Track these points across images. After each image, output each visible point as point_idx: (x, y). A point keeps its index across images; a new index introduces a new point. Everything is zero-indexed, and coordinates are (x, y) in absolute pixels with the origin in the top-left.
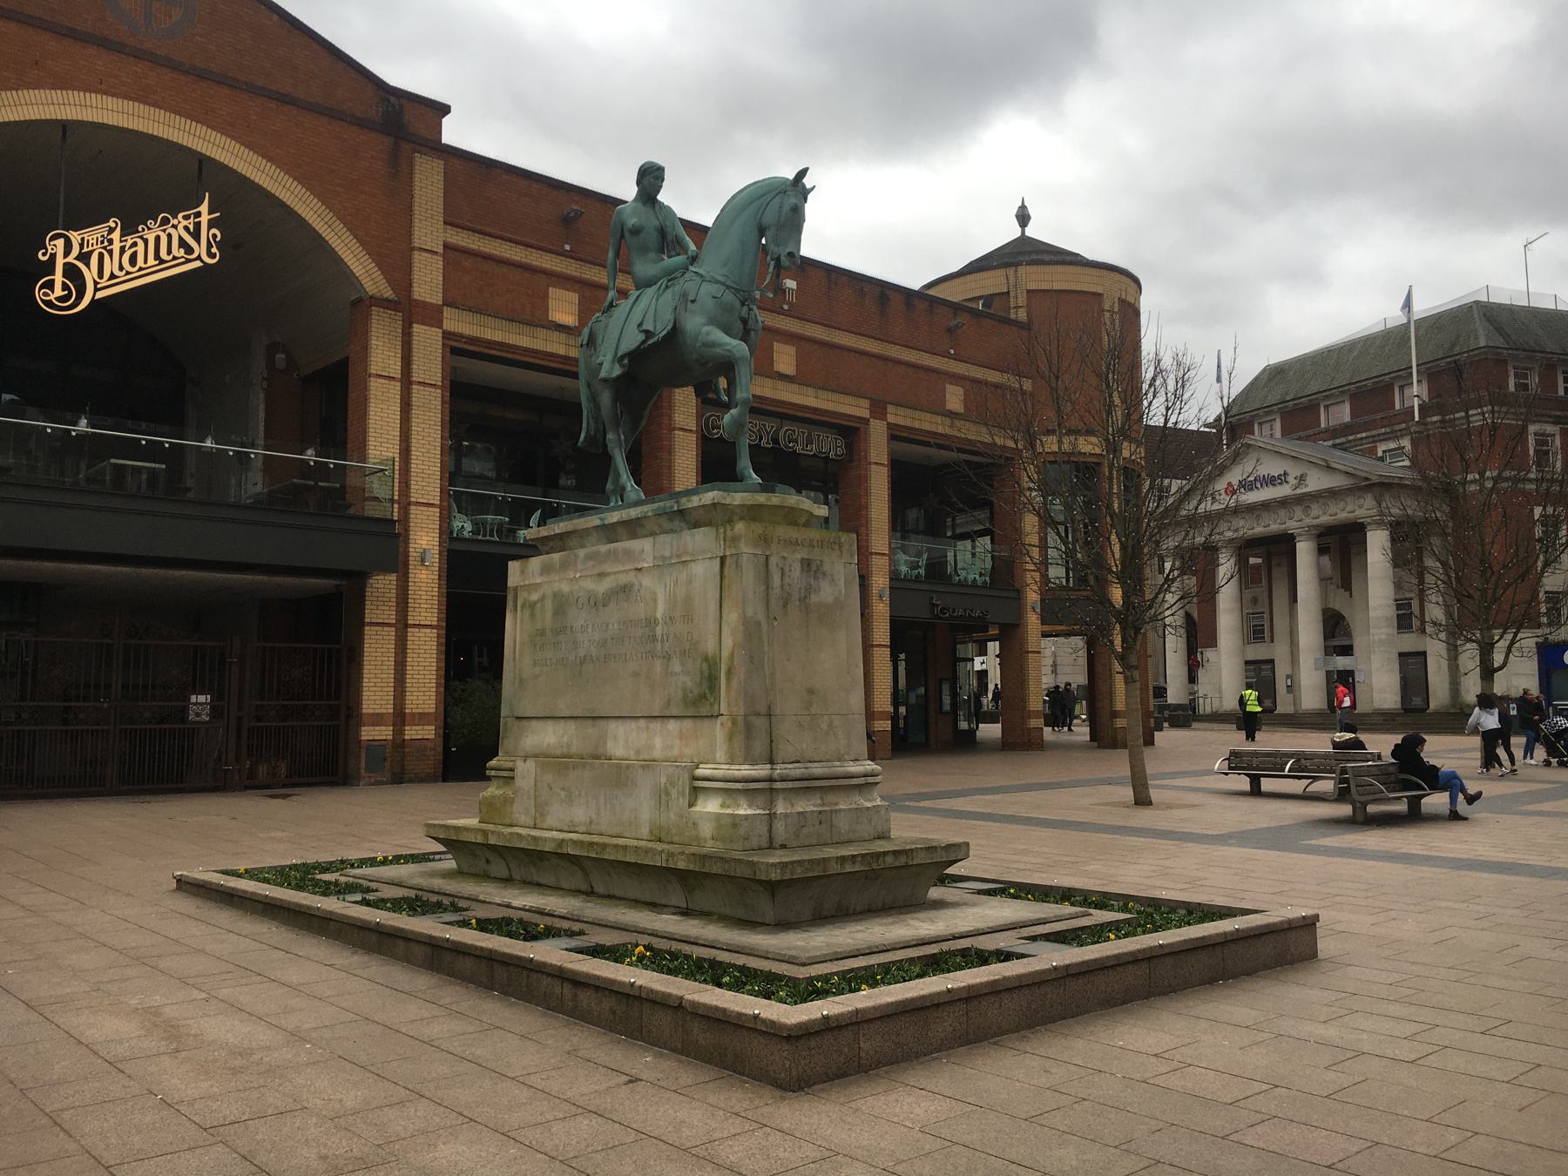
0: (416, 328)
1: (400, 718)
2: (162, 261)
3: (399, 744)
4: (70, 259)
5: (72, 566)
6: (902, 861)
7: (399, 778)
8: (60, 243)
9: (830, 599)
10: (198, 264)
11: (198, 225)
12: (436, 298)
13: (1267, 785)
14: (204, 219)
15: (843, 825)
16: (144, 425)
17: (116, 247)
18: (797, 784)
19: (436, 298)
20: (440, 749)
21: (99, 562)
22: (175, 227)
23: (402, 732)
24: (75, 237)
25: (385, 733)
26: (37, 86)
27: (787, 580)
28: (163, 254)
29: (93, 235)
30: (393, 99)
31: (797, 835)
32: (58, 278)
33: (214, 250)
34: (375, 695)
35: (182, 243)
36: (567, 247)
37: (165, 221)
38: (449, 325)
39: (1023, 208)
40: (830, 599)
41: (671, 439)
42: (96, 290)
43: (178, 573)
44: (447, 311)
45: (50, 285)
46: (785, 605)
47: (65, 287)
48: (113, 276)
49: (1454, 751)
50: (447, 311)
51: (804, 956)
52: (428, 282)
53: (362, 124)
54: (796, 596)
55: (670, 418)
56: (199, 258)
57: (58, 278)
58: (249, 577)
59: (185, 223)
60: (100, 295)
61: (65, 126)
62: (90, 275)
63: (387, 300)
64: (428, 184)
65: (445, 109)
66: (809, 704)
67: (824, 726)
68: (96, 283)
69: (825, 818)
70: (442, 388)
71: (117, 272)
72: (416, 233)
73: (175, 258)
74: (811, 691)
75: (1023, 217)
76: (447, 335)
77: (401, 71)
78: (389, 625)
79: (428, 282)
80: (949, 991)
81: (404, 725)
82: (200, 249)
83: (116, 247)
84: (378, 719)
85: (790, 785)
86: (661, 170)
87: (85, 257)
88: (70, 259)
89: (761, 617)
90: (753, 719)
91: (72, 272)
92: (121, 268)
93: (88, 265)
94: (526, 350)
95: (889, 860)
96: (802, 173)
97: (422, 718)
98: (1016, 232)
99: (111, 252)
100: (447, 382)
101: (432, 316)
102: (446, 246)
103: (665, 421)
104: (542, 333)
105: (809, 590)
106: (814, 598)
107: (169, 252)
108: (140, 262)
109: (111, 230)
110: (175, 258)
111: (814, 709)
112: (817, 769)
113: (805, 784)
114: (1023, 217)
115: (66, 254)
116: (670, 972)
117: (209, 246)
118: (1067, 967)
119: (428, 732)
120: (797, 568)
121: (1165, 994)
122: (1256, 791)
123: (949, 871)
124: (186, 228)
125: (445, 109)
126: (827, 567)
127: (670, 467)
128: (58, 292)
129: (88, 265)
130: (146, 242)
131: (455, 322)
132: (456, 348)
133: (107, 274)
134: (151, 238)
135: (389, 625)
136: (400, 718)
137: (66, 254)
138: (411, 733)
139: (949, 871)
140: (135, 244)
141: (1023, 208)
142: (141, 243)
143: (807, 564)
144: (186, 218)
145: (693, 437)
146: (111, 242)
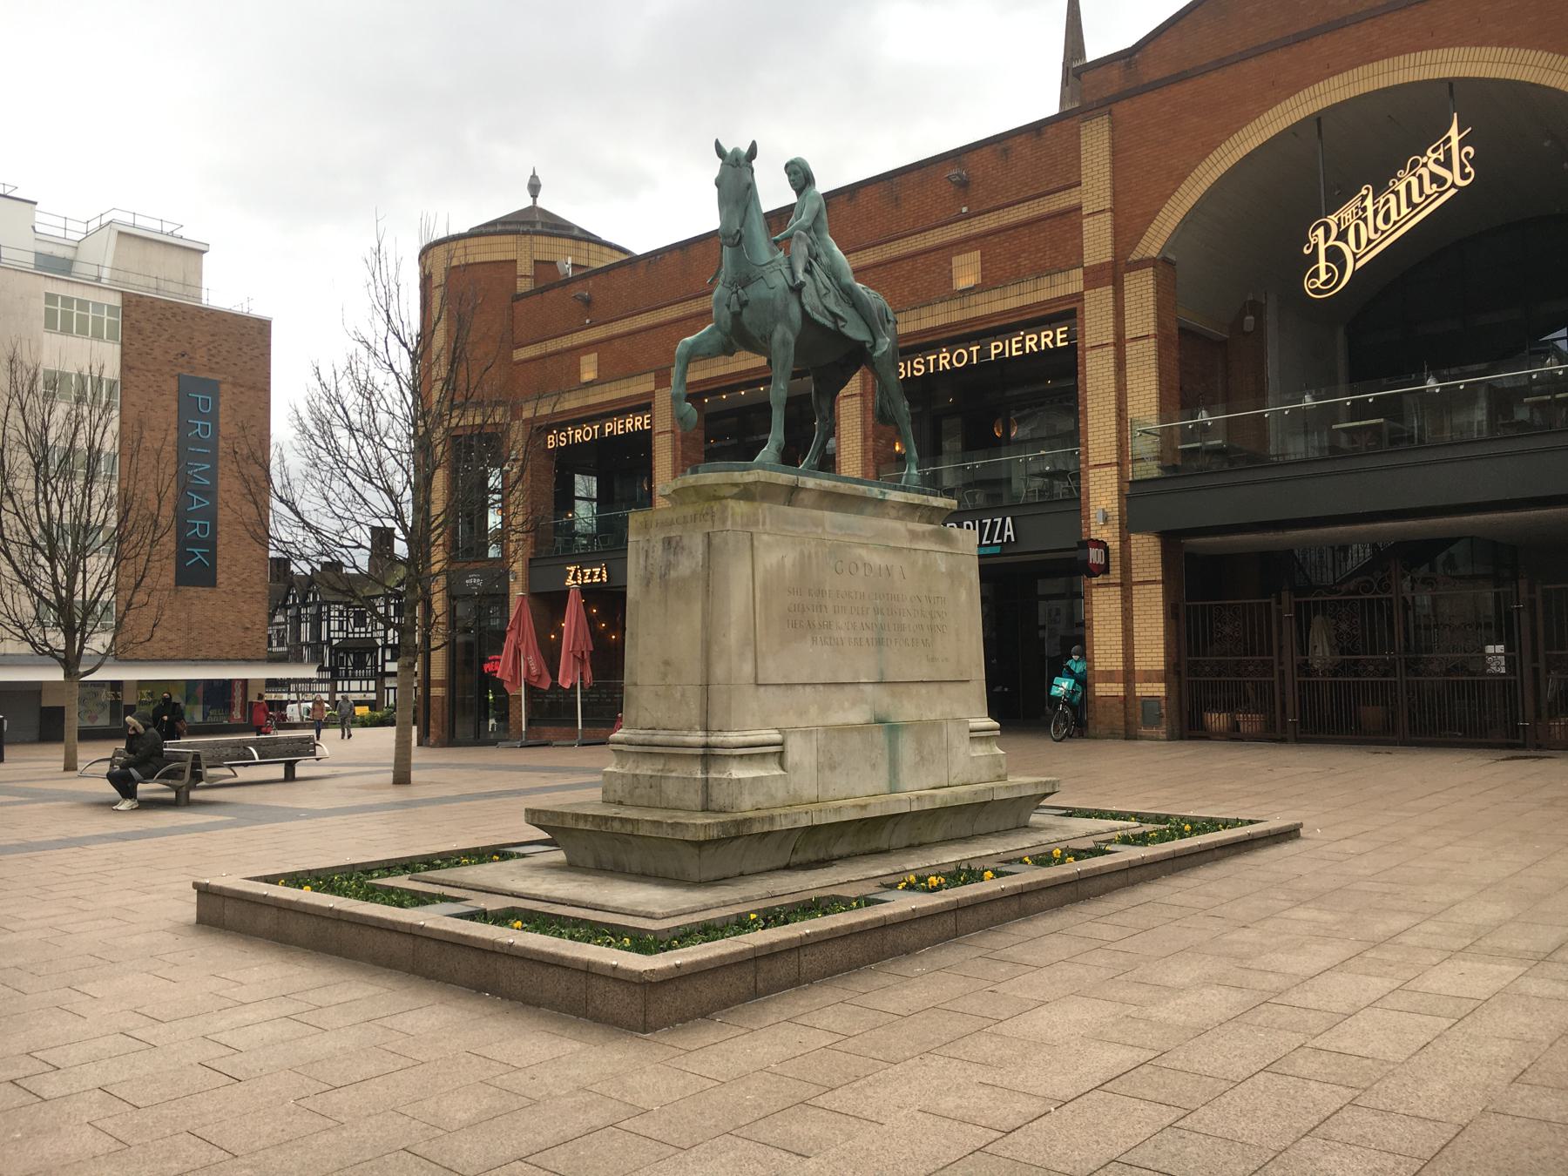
1: (1128, 675)
2: (1415, 206)
3: (1128, 699)
4: (1330, 243)
5: (1341, 528)
6: (628, 829)
7: (1130, 735)
8: (1321, 232)
10: (1453, 191)
11: (1448, 153)
13: (300, 771)
14: (1454, 143)
15: (671, 790)
16: (1385, 381)
17: (1370, 213)
18: (639, 749)
21: (1381, 520)
22: (1425, 165)
23: (1126, 689)
24: (1332, 220)
25: (1117, 689)
26: (1277, 102)
27: (651, 561)
28: (1416, 199)
29: (1347, 212)
31: (631, 794)
32: (1322, 264)
33: (1468, 169)
34: (1105, 649)
35: (1435, 178)
37: (1415, 164)
39: (534, 177)
40: (688, 572)
42: (1356, 261)
43: (1471, 518)
45: (1316, 274)
47: (1328, 270)
48: (1369, 241)
51: (658, 911)
54: (657, 574)
56: (1453, 185)
57: (1322, 264)
58: (1218, 539)
59: (1435, 156)
60: (1360, 264)
61: (1318, 119)
62: (1348, 250)
66: (665, 675)
67: (678, 695)
68: (1354, 254)
69: (655, 782)
71: (1373, 236)
73: (1428, 197)
74: (667, 663)
75: (534, 188)
77: (716, 190)
78: (1154, 582)
80: (678, 967)
82: (1454, 177)
83: (1370, 213)
84: (1109, 676)
85: (633, 749)
86: (787, 166)
87: (1342, 236)
88: (1330, 243)
91: (1335, 255)
92: (1376, 230)
93: (1346, 242)
95: (617, 826)
96: (720, 151)
97: (1149, 677)
98: (528, 202)
99: (1365, 220)
105: (669, 566)
106: (673, 574)
107: (1421, 192)
108: (1394, 217)
109: (1364, 198)
110: (1428, 197)
111: (670, 680)
112: (661, 737)
113: (646, 749)
114: (534, 188)
115: (1326, 240)
116: (786, 922)
117: (1463, 167)
118: (339, 911)
119: (1158, 689)
120: (659, 547)
121: (427, 978)
122: (290, 777)
123: (546, 836)
124: (1437, 161)
126: (686, 541)
128: (1323, 276)
129: (1346, 242)
130: (1397, 193)
133: (1364, 242)
134: (1402, 188)
135: (1154, 582)
136: (1128, 675)
137: (1326, 240)
138: (1143, 689)
139: (546, 836)
140: (1387, 201)
141: (534, 177)
142: (1392, 198)
143: (668, 542)
144: (1434, 151)
146: (1364, 209)
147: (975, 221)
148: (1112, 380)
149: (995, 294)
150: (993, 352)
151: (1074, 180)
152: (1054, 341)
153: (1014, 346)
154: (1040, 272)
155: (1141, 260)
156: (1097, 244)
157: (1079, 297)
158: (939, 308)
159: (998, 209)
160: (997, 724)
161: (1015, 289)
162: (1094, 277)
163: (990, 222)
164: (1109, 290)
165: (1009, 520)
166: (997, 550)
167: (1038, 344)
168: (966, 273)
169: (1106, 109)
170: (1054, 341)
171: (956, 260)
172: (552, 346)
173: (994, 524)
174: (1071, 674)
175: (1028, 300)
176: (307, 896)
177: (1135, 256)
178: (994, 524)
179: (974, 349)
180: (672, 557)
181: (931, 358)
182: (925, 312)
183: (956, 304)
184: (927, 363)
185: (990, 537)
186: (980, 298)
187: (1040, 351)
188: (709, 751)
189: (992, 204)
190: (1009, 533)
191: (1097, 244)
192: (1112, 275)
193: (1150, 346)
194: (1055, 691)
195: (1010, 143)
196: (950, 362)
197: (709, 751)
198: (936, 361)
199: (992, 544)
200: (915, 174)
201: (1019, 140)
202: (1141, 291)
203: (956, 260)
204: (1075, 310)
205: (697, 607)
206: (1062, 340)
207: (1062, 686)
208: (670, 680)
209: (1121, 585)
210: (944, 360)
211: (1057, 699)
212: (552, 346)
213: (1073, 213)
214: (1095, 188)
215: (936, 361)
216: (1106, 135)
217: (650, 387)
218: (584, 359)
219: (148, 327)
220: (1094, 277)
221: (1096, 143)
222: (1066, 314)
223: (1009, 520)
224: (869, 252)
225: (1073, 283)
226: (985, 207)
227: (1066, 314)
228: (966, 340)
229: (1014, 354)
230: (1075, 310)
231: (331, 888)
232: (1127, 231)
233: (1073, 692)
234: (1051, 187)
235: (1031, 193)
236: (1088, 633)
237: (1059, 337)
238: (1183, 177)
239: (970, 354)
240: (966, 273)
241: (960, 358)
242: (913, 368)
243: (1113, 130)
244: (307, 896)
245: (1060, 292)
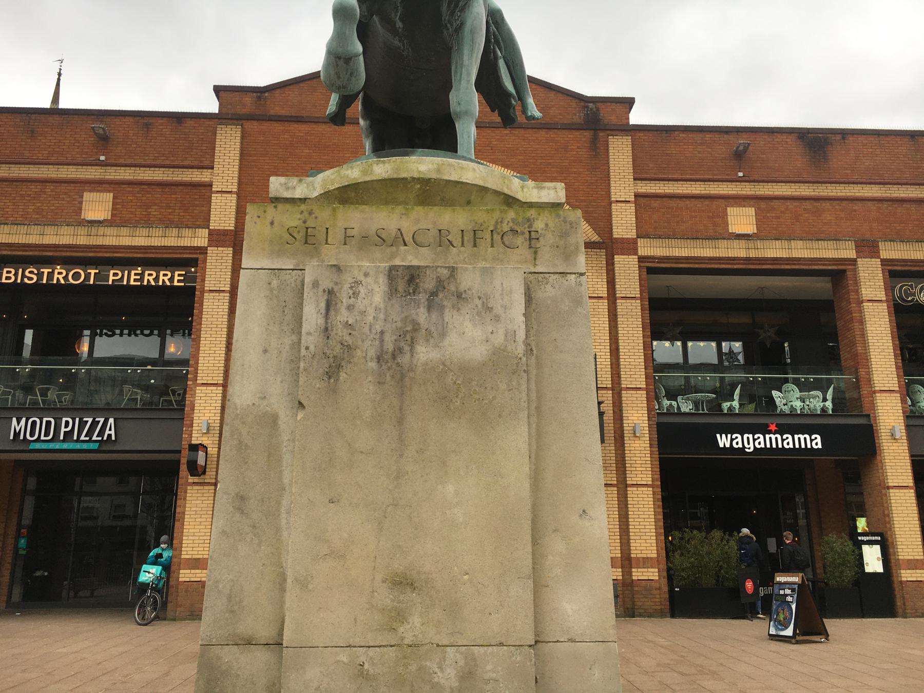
0: (617, 258)
9: (479, 353)
12: (632, 234)
19: (632, 234)
20: (665, 589)
23: (630, 573)
27: (343, 316)
30: (591, 105)
36: (741, 174)
38: (642, 251)
41: (861, 311)
44: (640, 242)
46: (332, 372)
49: (540, 397)
50: (640, 242)
52: (624, 223)
53: (569, 127)
55: (857, 292)
63: (594, 243)
64: (620, 153)
65: (629, 103)
66: (399, 616)
70: (641, 299)
72: (613, 190)
76: (641, 259)
79: (624, 223)
81: (631, 568)
89: (279, 405)
90: (228, 655)
94: (711, 259)
97: (645, 562)
100: (646, 295)
101: (629, 247)
102: (637, 196)
103: (853, 296)
104: (723, 243)
105: (410, 334)
106: (424, 353)
111: (414, 628)
119: (652, 574)
125: (629, 103)
126: (469, 280)
127: (863, 335)
131: (647, 248)
132: (651, 269)
143: (405, 282)
145: (884, 306)
147: (111, 170)
148: (226, 318)
150: (111, 278)
151: (206, 163)
152: (171, 279)
153: (133, 277)
156: (222, 213)
157: (203, 250)
158: (65, 230)
159: (135, 166)
161: (145, 232)
162: (218, 238)
165: (111, 421)
166: (94, 446)
167: (156, 279)
168: (97, 207)
169: (240, 122)
170: (171, 279)
171: (87, 196)
173: (95, 424)
174: (156, 561)
175: (156, 242)
178: (95, 424)
179: (93, 272)
180: (422, 315)
181: (46, 271)
183: (83, 231)
184: (40, 275)
185: (90, 433)
186: (109, 231)
187: (157, 287)
189: (129, 162)
190: (110, 432)
194: (144, 577)
195: (152, 120)
196: (66, 278)
198: (51, 275)
199: (90, 441)
201: (160, 121)
203: (87, 196)
204: (196, 260)
205: (516, 439)
206: (179, 281)
207: (149, 573)
208: (414, 628)
210: (60, 275)
211: (145, 586)
215: (51, 275)
216: (238, 140)
220: (218, 238)
221: (228, 145)
222: (189, 260)
223: (111, 421)
225: (200, 238)
226: (122, 161)
227: (189, 260)
228: (86, 263)
229: (132, 283)
230: (196, 260)
233: (159, 578)
234: (186, 163)
235: (167, 162)
236: (177, 524)
237: (176, 278)
239: (88, 276)
241: (76, 276)
242: (23, 276)
243: (243, 138)
245: (186, 242)
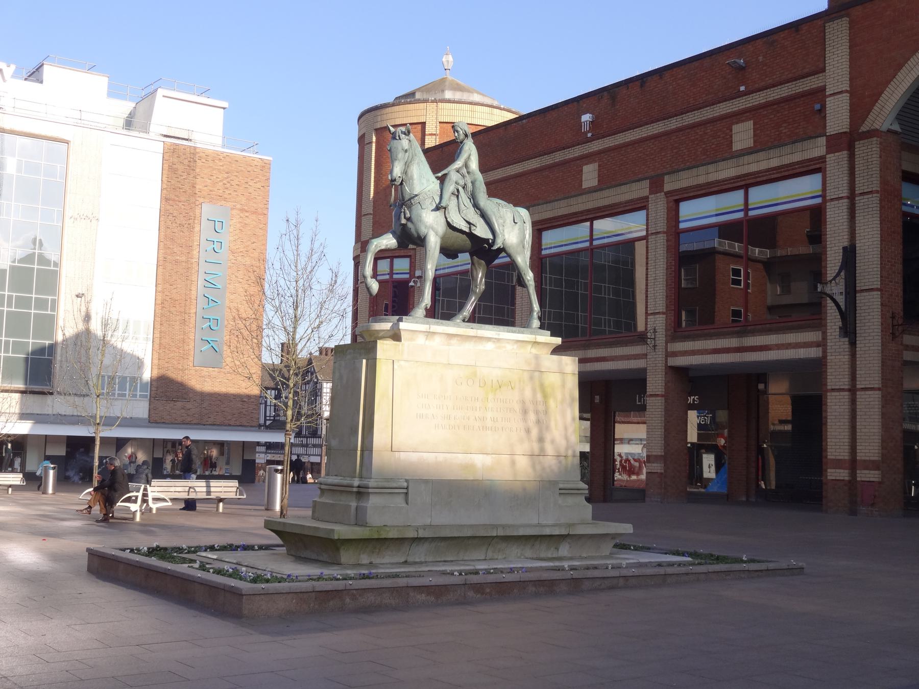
1: (853, 464)
3: (852, 483)
25: (843, 474)
84: (838, 464)
97: (871, 465)
135: (843, 390)
136: (853, 464)
138: (864, 475)
149: (762, 155)
154: (797, 139)
155: (868, 131)
156: (838, 116)
160: (586, 486)
162: (835, 143)
163: (596, 146)
164: (845, 154)
172: (559, 157)
176: (153, 561)
177: (863, 129)
182: (711, 168)
188: (362, 490)
191: (838, 116)
192: (846, 142)
193: (875, 199)
197: (362, 490)
200: (696, 64)
202: (869, 154)
209: (849, 390)
212: (559, 157)
213: (819, 94)
214: (837, 72)
217: (646, 192)
218: (586, 169)
219: (180, 167)
220: (835, 143)
224: (673, 120)
231: (162, 558)
232: (861, 105)
238: (900, 67)
240: (590, 175)
244: (153, 561)
